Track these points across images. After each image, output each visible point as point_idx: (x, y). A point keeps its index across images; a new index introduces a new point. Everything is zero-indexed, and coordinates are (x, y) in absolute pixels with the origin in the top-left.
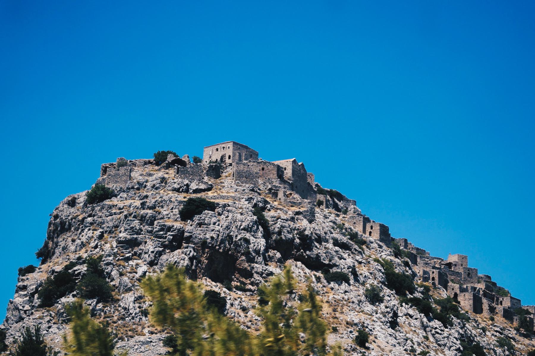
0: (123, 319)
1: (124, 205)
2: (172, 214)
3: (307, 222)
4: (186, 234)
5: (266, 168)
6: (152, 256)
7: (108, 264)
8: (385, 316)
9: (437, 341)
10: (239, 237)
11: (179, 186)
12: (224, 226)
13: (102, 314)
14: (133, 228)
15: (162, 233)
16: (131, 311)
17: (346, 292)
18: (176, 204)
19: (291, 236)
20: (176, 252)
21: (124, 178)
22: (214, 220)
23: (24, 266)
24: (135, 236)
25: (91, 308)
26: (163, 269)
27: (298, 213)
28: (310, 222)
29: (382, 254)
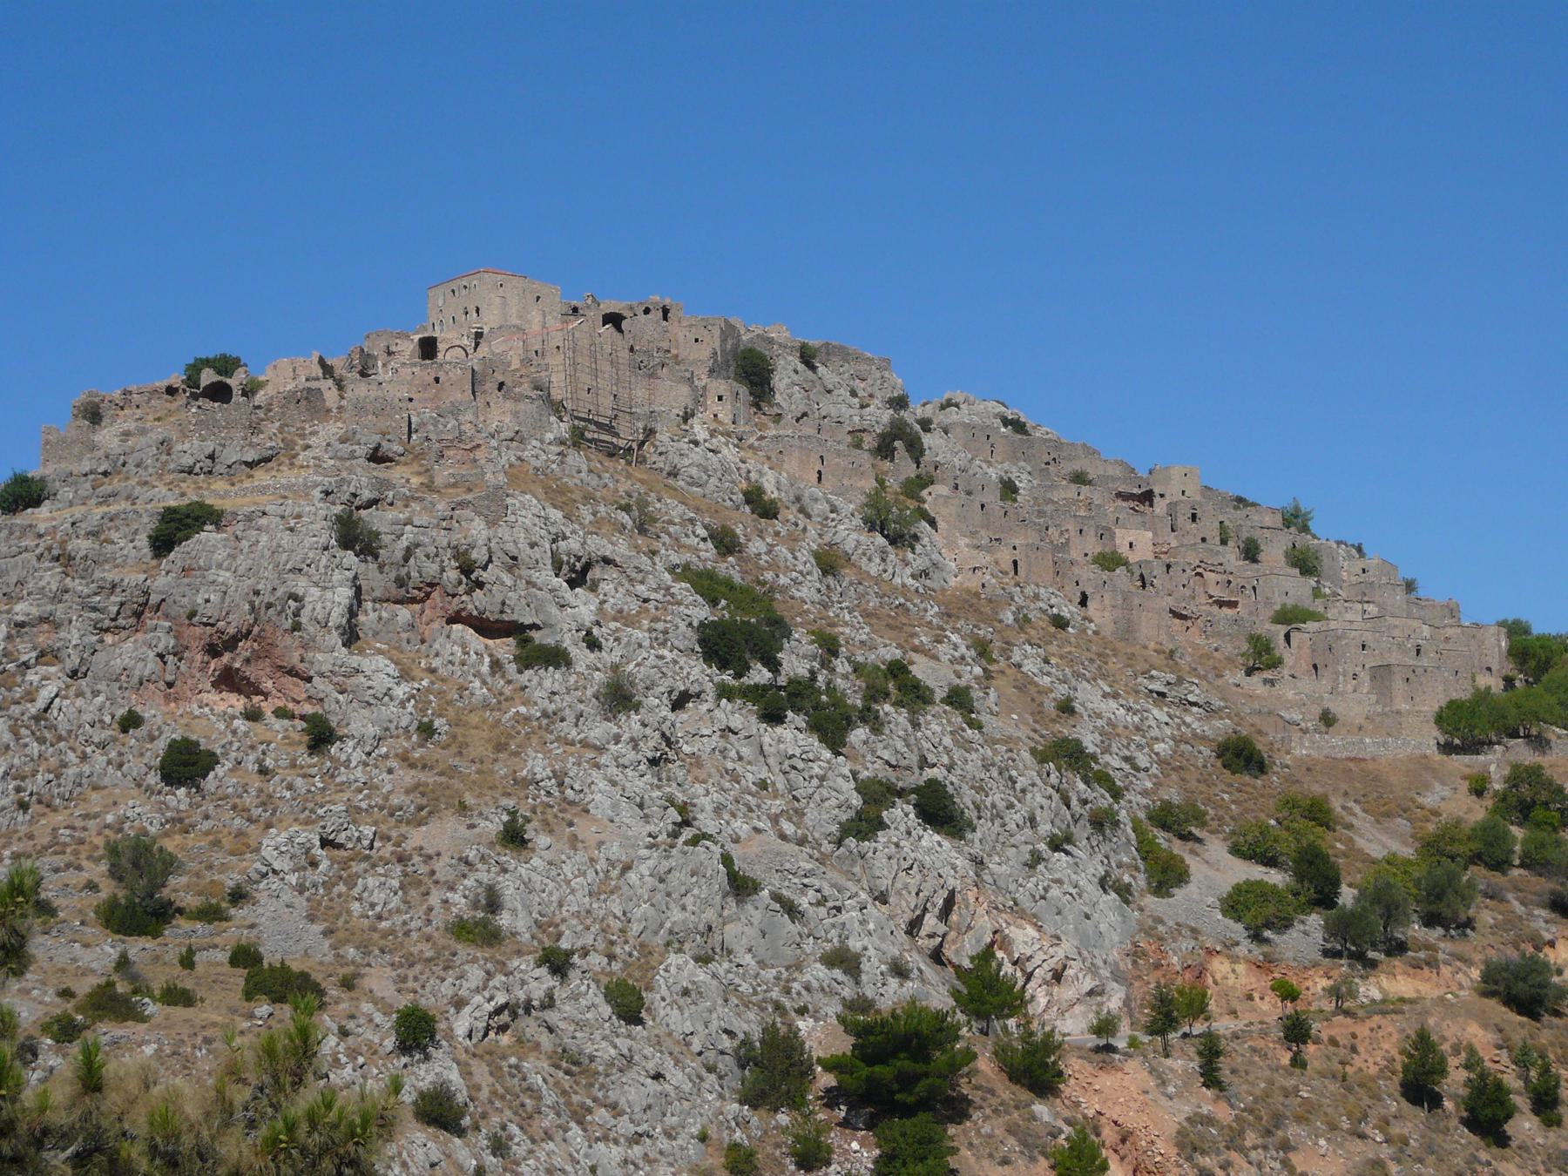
2: (131, 545)
3: (483, 525)
5: (441, 375)
8: (636, 748)
11: (191, 461)
15: (98, 598)
26: (99, 687)
27: (462, 505)
28: (492, 523)
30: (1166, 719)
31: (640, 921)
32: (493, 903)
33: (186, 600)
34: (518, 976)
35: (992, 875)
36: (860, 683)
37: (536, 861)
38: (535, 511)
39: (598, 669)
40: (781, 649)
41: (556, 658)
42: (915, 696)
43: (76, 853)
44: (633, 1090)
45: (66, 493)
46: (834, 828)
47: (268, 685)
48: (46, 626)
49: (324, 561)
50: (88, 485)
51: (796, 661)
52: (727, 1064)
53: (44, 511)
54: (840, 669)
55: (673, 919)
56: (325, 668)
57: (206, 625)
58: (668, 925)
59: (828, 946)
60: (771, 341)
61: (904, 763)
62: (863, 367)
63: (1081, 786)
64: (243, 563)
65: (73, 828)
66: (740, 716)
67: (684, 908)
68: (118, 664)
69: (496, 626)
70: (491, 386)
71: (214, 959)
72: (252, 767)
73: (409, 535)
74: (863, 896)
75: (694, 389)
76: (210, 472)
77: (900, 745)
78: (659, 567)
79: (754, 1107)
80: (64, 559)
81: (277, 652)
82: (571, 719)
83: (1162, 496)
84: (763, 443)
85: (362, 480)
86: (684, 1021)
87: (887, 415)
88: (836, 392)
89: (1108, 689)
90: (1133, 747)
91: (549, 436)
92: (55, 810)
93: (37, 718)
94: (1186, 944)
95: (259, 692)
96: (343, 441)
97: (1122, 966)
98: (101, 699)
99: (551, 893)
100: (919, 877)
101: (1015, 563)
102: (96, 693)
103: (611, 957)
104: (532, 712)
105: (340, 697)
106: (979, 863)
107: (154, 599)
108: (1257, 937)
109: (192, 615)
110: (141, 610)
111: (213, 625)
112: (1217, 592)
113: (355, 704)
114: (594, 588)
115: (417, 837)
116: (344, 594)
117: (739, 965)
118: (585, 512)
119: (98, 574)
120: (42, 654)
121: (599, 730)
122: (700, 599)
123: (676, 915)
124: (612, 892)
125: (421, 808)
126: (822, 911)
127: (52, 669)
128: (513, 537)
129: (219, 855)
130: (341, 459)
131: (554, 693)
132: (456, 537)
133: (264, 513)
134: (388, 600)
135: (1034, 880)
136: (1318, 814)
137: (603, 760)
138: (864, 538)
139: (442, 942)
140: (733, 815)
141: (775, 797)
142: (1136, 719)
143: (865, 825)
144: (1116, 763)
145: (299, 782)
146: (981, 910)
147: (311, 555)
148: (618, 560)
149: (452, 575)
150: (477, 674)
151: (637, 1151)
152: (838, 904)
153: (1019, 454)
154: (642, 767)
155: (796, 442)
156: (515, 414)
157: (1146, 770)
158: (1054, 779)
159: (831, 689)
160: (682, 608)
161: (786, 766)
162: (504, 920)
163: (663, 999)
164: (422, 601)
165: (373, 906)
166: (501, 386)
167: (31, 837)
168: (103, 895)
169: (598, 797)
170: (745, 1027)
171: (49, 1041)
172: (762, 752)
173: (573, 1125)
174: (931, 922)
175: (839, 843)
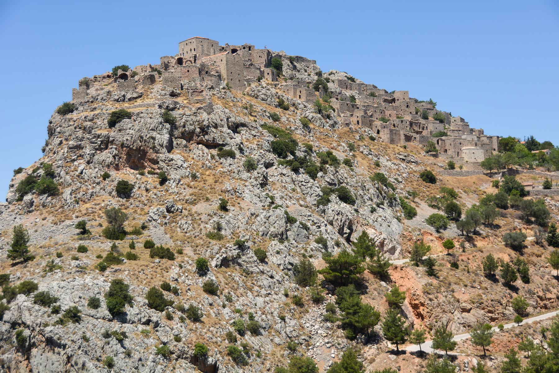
0: (62, 207)
1: (77, 118)
2: (103, 123)
3: (206, 114)
4: (111, 139)
5: (190, 70)
6: (88, 156)
7: (58, 167)
8: (256, 180)
9: (302, 191)
10: (148, 137)
11: (118, 98)
12: (137, 130)
13: (50, 205)
14: (77, 137)
15: (94, 140)
16: (68, 201)
17: (230, 165)
18: (107, 116)
19: (193, 127)
20: (104, 153)
21: (83, 95)
22: (130, 126)
23: (17, 169)
24: (79, 143)
25: (42, 201)
26: (96, 166)
27: (199, 108)
28: (209, 114)
29: (307, 112)
30: (405, 167)
32: (219, 228)
34: (229, 248)
36: (320, 159)
37: (230, 215)
41: (231, 155)
42: (335, 162)
43: (94, 216)
44: (265, 281)
45: (81, 108)
52: (291, 273)
53: (75, 112)
54: (313, 155)
55: (271, 231)
58: (270, 232)
59: (317, 237)
64: (137, 128)
65: (93, 208)
66: (287, 171)
68: (101, 159)
71: (140, 246)
72: (143, 188)
73: (185, 118)
74: (326, 222)
75: (261, 71)
77: (332, 177)
84: (283, 87)
85: (169, 101)
87: (316, 78)
89: (388, 158)
90: (397, 175)
91: (221, 87)
92: (86, 203)
96: (162, 90)
98: (97, 169)
100: (341, 216)
101: (358, 121)
102: (95, 168)
103: (255, 243)
104: (225, 170)
105: (168, 167)
106: (356, 211)
108: (438, 232)
110: (106, 143)
115: (194, 209)
116: (167, 136)
117: (291, 244)
121: (245, 175)
122: (271, 135)
123: (272, 229)
126: (314, 227)
127: (82, 161)
128: (215, 118)
129: (137, 215)
130: (162, 95)
131: (230, 165)
132: (198, 118)
133: (142, 113)
136: (452, 194)
137: (247, 184)
138: (314, 115)
139: (206, 240)
142: (397, 167)
143: (324, 201)
144: (393, 180)
146: (359, 226)
151: (267, 299)
154: (259, 186)
157: (401, 182)
159: (311, 161)
160: (266, 138)
162: (223, 232)
168: (104, 228)
169: (246, 195)
171: (97, 271)
173: (249, 292)
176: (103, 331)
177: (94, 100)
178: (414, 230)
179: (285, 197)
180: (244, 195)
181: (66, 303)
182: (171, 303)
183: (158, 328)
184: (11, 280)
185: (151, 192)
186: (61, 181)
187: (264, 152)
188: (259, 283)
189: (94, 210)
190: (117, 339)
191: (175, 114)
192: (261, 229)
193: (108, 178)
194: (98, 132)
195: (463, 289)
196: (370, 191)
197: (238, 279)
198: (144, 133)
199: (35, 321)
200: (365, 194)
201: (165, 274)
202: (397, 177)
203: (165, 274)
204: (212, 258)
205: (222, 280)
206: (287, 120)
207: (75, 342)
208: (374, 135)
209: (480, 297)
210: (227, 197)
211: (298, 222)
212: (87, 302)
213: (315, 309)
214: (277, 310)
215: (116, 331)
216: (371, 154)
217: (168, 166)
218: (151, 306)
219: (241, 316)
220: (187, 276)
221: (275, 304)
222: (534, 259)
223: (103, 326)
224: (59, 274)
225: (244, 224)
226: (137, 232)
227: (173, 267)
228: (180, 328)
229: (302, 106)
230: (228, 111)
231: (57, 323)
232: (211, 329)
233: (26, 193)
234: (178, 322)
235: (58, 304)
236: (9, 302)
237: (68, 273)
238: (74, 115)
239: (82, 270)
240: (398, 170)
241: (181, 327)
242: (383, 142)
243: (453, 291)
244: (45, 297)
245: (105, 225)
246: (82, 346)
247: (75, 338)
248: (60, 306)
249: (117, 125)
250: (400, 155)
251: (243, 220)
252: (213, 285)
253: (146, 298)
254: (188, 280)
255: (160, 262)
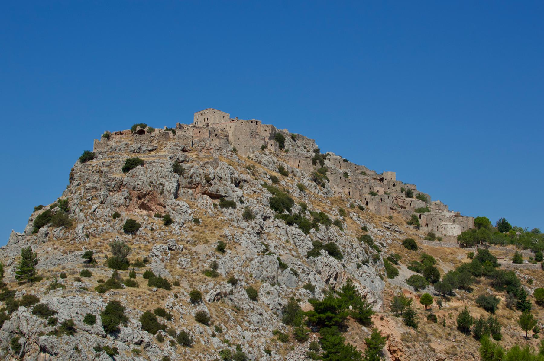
0: (74, 239)
3: (212, 169)
5: (201, 130)
9: (295, 243)
11: (134, 149)
15: (109, 183)
16: (79, 235)
17: (231, 214)
27: (207, 163)
28: (215, 168)
31: (255, 274)
32: (215, 266)
33: (133, 184)
35: (347, 269)
37: (227, 256)
38: (227, 166)
39: (243, 208)
40: (291, 207)
41: (232, 205)
42: (327, 221)
45: (100, 157)
46: (306, 254)
47: (153, 208)
48: (94, 190)
49: (170, 175)
50: (106, 155)
51: (296, 209)
52: (279, 313)
53: (94, 160)
54: (307, 213)
56: (170, 204)
57: (138, 190)
58: (262, 276)
60: (284, 133)
61: (324, 239)
62: (308, 141)
63: (370, 248)
64: (148, 174)
65: (101, 242)
66: (281, 223)
67: (267, 271)
68: (113, 200)
69: (215, 196)
70: (214, 135)
75: (265, 142)
76: (139, 152)
77: (323, 234)
78: (259, 184)
79: (287, 324)
80: (100, 172)
81: (157, 199)
82: (236, 221)
83: (386, 179)
84: (283, 157)
85: (180, 155)
86: (268, 300)
87: (314, 154)
88: (301, 147)
89: (375, 226)
91: (228, 149)
93: (91, 214)
94: (399, 291)
95: (151, 210)
96: (174, 146)
97: (381, 296)
99: (231, 265)
100: (329, 268)
101: (349, 192)
102: (107, 207)
106: (344, 266)
107: (124, 183)
108: (416, 290)
109: (134, 188)
110: (120, 186)
111: (140, 191)
112: (401, 204)
113: (177, 214)
114: (241, 188)
115: (194, 249)
116: (175, 184)
118: (239, 168)
119: (109, 176)
120: (93, 198)
121: (244, 224)
122: (270, 192)
124: (247, 266)
125: (196, 241)
126: (304, 275)
127: (96, 201)
131: (231, 214)
132: (206, 171)
133: (154, 162)
134: (186, 187)
135: (358, 271)
137: (244, 232)
138: (311, 183)
140: (279, 249)
141: (290, 245)
142: (382, 234)
143: (314, 253)
145: (162, 233)
147: (167, 173)
148: (248, 181)
149: (204, 181)
150: (210, 208)
151: (255, 334)
152: (308, 273)
153: (348, 167)
155: (293, 157)
156: (220, 143)
157: (386, 247)
158: (363, 245)
161: (293, 237)
162: (219, 271)
163: (262, 295)
164: (195, 188)
165: (182, 266)
166: (216, 135)
167: (89, 244)
169: (243, 242)
170: (284, 303)
171: (97, 293)
172: (287, 233)
173: (238, 325)
174: (332, 280)
175: (308, 258)
176: (95, 345)
177: (114, 150)
178: (395, 288)
179: (279, 247)
180: (241, 241)
181: (63, 316)
182: (164, 327)
183: (148, 348)
184: (16, 296)
185: (156, 232)
186: (75, 217)
187: (262, 206)
188: (249, 319)
189: (102, 244)
190: (108, 354)
191: (184, 166)
192: (254, 272)
193: (118, 217)
194: (113, 176)
195: (439, 340)
196: (357, 250)
197: (229, 314)
198: (155, 179)
199: (31, 330)
200: (352, 252)
201: (161, 302)
202: (382, 241)
203: (161, 302)
204: (207, 293)
205: (213, 310)
206: (286, 184)
207: (67, 352)
208: (364, 206)
209: (453, 349)
210: (224, 240)
211: (289, 269)
212: (84, 318)
213: (300, 347)
214: (264, 344)
215: (108, 346)
216: (359, 220)
217: (174, 210)
218: (144, 328)
219: (230, 346)
220: (181, 306)
221: (262, 339)
222: (505, 321)
223: (94, 340)
224: (60, 291)
225: (239, 266)
226: (139, 264)
227: (169, 296)
228: (170, 351)
229: (300, 174)
230: (233, 168)
231: (51, 333)
232: (200, 355)
233: (43, 226)
234: (168, 345)
235: (55, 316)
236: (11, 312)
237: (69, 291)
238: (94, 162)
239: (84, 290)
240: (383, 236)
241: (171, 349)
242: (370, 212)
243: (429, 341)
244: (43, 309)
245: (110, 255)
246: (73, 356)
247: (67, 348)
248: (57, 318)
249: (131, 172)
250: (386, 224)
251: (239, 262)
252: (206, 315)
253: (140, 320)
254: (182, 309)
255: (157, 290)
